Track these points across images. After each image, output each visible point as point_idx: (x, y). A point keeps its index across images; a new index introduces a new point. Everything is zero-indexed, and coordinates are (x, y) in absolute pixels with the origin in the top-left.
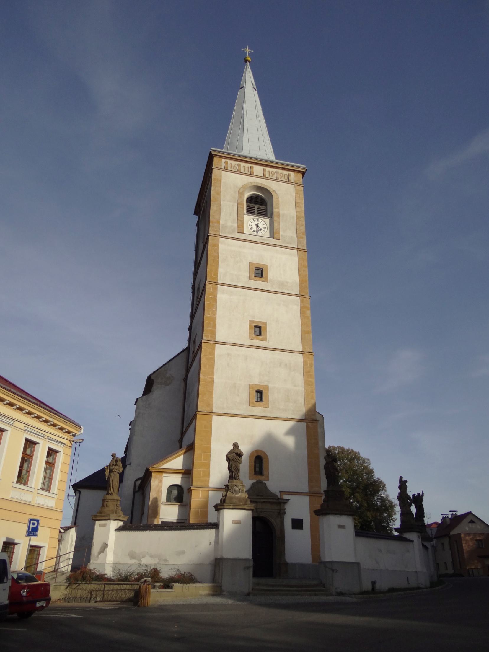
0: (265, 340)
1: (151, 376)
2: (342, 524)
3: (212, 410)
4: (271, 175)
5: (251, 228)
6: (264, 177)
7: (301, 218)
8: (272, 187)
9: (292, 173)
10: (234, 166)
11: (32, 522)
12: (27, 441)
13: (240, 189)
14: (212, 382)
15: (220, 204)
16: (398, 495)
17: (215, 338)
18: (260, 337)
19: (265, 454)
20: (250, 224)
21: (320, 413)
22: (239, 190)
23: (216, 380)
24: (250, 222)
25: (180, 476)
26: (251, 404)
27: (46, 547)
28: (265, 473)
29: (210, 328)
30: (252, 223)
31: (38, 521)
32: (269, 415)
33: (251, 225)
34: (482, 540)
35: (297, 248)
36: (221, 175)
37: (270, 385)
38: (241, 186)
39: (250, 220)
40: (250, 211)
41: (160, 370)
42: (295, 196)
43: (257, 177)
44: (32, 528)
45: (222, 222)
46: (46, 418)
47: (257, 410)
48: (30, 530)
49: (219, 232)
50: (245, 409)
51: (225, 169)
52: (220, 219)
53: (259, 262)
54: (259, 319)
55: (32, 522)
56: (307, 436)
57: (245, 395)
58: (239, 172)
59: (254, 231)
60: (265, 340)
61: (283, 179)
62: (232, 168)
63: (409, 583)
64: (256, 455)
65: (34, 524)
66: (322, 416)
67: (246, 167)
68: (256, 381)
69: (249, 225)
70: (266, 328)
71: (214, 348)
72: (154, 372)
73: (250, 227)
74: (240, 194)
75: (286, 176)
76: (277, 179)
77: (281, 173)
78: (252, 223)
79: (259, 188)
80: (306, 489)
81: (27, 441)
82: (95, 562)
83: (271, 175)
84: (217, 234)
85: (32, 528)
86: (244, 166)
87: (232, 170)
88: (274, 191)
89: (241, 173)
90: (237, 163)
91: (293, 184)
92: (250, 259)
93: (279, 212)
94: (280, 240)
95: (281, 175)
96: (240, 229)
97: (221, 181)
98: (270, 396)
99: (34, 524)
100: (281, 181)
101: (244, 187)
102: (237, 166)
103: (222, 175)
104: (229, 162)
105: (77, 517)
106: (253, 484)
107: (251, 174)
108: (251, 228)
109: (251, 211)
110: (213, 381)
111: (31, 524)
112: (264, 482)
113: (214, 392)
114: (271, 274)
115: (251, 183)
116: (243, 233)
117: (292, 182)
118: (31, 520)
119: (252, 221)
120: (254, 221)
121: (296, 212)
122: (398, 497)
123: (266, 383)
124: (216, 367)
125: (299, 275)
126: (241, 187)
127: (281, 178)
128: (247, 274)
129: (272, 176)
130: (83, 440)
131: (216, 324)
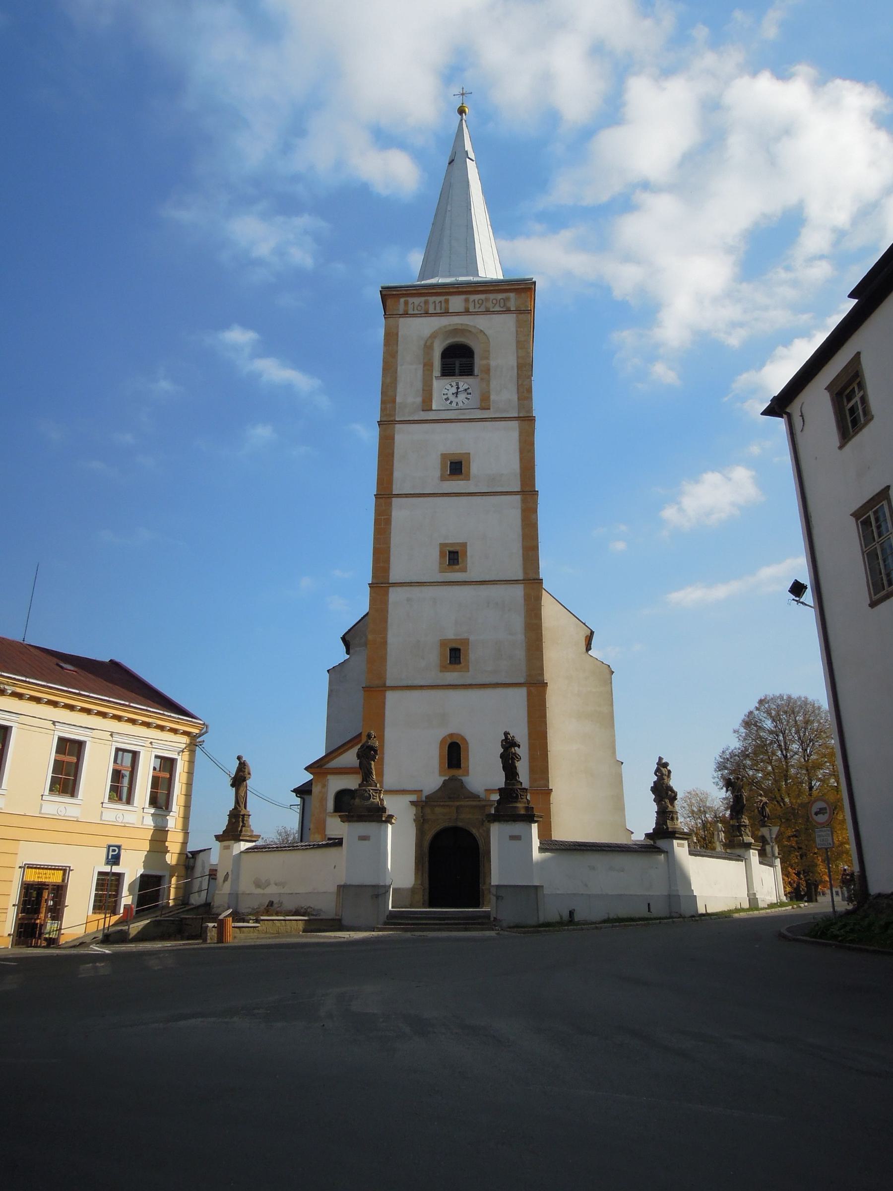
0: (464, 570)
1: (346, 637)
2: (517, 833)
3: (385, 684)
4: (477, 306)
5: (447, 399)
6: (467, 312)
7: (525, 367)
8: (478, 326)
9: (512, 295)
10: (419, 305)
11: (111, 848)
13: (427, 340)
14: (384, 643)
15: (396, 371)
16: (653, 785)
17: (388, 579)
18: (457, 567)
19: (458, 735)
20: (445, 391)
21: (604, 663)
22: (426, 343)
24: (446, 389)
26: (443, 668)
27: (166, 877)
28: (462, 765)
30: (448, 390)
31: (119, 847)
32: (469, 682)
33: (447, 394)
34: (217, 864)
35: (519, 417)
36: (398, 325)
39: (443, 387)
40: (447, 371)
41: (358, 625)
42: (517, 331)
44: (112, 855)
45: (398, 400)
46: (143, 720)
47: (452, 677)
49: (395, 415)
50: (435, 676)
51: (406, 314)
52: (396, 396)
53: (455, 449)
54: (454, 538)
55: (111, 848)
56: (529, 706)
57: (433, 656)
58: (427, 314)
59: (451, 403)
60: (464, 570)
61: (497, 308)
62: (415, 309)
63: (649, 911)
64: (449, 741)
66: (609, 666)
67: (437, 302)
69: (444, 394)
71: (387, 593)
72: (350, 630)
73: (445, 397)
74: (428, 348)
75: (502, 301)
76: (488, 312)
77: (494, 299)
78: (448, 390)
79: (456, 331)
82: (220, 892)
83: (477, 306)
84: (392, 419)
85: (112, 855)
86: (474, 300)
87: (416, 313)
88: (481, 331)
89: (430, 315)
90: (423, 299)
91: (514, 313)
92: (443, 449)
94: (489, 409)
96: (427, 405)
97: (397, 334)
98: (473, 655)
100: (494, 312)
101: (433, 336)
102: (422, 304)
103: (400, 325)
104: (411, 300)
105: (304, 833)
106: (445, 782)
107: (446, 313)
108: (447, 399)
110: (386, 642)
111: (111, 851)
112: (459, 778)
113: (388, 658)
114: (475, 468)
115: (445, 327)
117: (512, 309)
118: (109, 846)
119: (448, 387)
120: (452, 386)
121: (518, 357)
122: (652, 787)
123: (465, 636)
124: (390, 621)
125: (521, 459)
126: (430, 337)
127: (493, 308)
128: (438, 473)
129: (479, 307)
130: (204, 741)
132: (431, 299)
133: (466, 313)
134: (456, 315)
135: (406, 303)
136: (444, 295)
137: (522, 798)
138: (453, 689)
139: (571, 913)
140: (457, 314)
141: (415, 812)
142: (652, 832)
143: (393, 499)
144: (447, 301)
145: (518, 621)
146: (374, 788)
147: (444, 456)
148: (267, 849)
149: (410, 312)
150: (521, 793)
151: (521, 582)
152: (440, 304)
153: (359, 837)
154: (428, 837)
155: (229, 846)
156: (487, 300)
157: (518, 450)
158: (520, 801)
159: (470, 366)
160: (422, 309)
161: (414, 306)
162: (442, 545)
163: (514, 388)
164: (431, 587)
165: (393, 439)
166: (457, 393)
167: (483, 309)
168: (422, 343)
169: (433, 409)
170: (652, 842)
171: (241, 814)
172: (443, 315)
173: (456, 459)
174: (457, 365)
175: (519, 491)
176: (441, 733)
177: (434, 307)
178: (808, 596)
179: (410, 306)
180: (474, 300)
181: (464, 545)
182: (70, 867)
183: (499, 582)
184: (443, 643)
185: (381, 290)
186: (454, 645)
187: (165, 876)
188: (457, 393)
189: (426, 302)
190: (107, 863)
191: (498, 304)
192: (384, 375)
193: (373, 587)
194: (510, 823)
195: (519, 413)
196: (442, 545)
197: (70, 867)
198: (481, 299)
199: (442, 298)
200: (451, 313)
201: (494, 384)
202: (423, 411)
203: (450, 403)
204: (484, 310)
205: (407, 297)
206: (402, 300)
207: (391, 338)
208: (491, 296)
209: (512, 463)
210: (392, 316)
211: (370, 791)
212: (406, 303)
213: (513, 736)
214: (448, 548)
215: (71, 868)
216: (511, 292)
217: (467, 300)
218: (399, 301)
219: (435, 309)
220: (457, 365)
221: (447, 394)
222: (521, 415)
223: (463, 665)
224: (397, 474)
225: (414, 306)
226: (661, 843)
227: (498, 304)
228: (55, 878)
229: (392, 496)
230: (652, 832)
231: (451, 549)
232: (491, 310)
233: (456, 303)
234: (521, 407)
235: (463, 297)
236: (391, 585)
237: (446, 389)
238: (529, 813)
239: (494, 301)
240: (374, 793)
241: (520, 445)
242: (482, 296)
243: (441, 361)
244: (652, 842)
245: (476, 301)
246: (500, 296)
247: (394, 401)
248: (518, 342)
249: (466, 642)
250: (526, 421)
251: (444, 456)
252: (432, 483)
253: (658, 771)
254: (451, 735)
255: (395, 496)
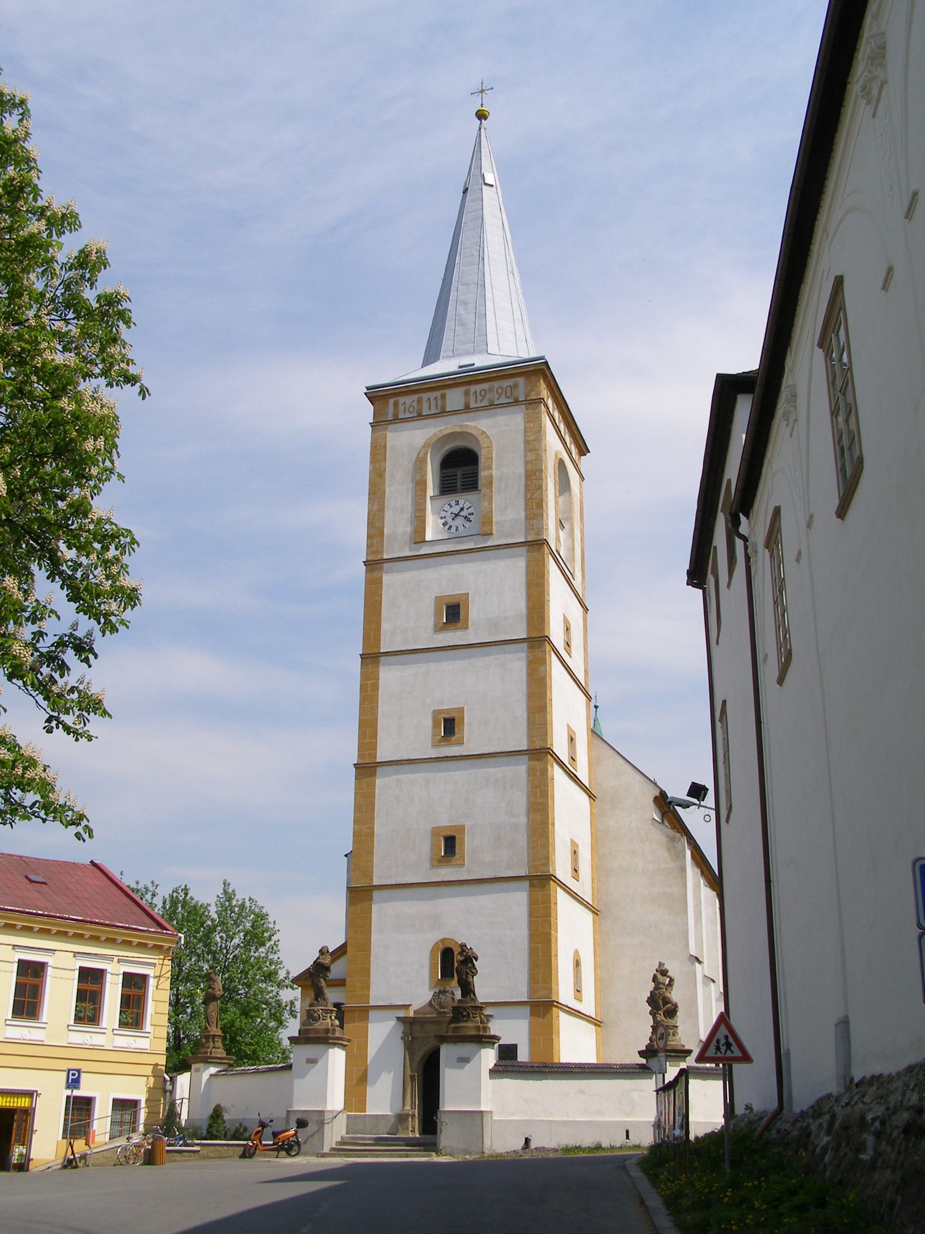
0: (460, 742)
4: (479, 398)
6: (467, 408)
7: (535, 475)
9: (521, 381)
10: (411, 406)
11: (71, 1072)
12: (24, 966)
22: (419, 453)
23: (377, 830)
24: (444, 510)
25: (372, 1003)
29: (368, 740)
31: (79, 1071)
37: (468, 824)
38: (422, 444)
42: (525, 428)
43: (452, 413)
44: (72, 1079)
47: (446, 873)
48: (70, 1081)
52: (384, 527)
53: (451, 590)
57: (424, 847)
58: (420, 416)
60: (460, 742)
61: (503, 400)
62: (407, 411)
63: (627, 1137)
64: (442, 947)
65: (74, 1075)
67: (432, 399)
68: (444, 820)
70: (463, 719)
74: (420, 464)
76: (492, 406)
79: (453, 436)
80: (522, 995)
81: (24, 966)
83: (479, 398)
84: (379, 557)
85: (72, 1079)
86: (476, 392)
90: (415, 397)
92: (437, 591)
93: (491, 476)
95: (500, 391)
98: (469, 845)
99: (74, 1075)
102: (415, 404)
104: (401, 400)
109: (450, 484)
116: (424, 541)
117: (520, 400)
119: (447, 507)
121: (526, 463)
126: (423, 447)
128: (430, 623)
131: (376, 731)
132: (425, 396)
133: (466, 411)
134: (454, 414)
135: (396, 405)
136: (439, 390)
137: (474, 1017)
138: (446, 885)
139: (527, 1141)
140: (455, 412)
141: (402, 1030)
142: (645, 1049)
143: (381, 658)
144: (443, 397)
145: (520, 799)
146: (323, 1008)
147: (438, 599)
148: (234, 1072)
149: (401, 416)
150: (473, 1011)
151: (525, 753)
152: (435, 400)
153: (307, 1059)
154: (418, 1058)
155: (199, 1068)
156: (491, 390)
157: (524, 585)
158: (471, 1020)
159: (475, 480)
160: (414, 410)
161: (405, 408)
162: (436, 713)
163: (521, 503)
164: (423, 764)
165: (381, 583)
166: (457, 515)
167: (485, 403)
168: (414, 456)
169: (427, 539)
170: (644, 1061)
171: (211, 1034)
172: (438, 415)
173: (453, 601)
174: (459, 476)
175: (525, 637)
176: (432, 937)
177: (428, 406)
178: (710, 800)
179: (401, 408)
180: (476, 392)
181: (461, 710)
182: (37, 1091)
183: (500, 755)
184: (435, 832)
185: (366, 391)
186: (449, 833)
187: (140, 1100)
188: (457, 515)
189: (420, 401)
190: (68, 1087)
191: (503, 395)
192: (370, 500)
193: (358, 768)
194: (458, 1044)
195: (526, 537)
196: (436, 713)
197: (37, 1091)
198: (485, 390)
199: (438, 394)
200: (448, 412)
201: (498, 501)
202: (415, 543)
203: (448, 529)
204: (488, 404)
205: (397, 396)
206: (391, 401)
207: (378, 452)
208: (496, 384)
209: (517, 603)
210: (379, 424)
211: (319, 1011)
212: (396, 405)
213: (471, 948)
214: (443, 716)
215: (38, 1092)
216: (518, 377)
217: (467, 394)
218: (388, 403)
219: (430, 409)
220: (459, 476)
221: (445, 517)
222: (529, 539)
223: (457, 856)
224: (385, 626)
225: (405, 408)
226: (653, 1063)
227: (503, 395)
228: (24, 1102)
229: (379, 655)
230: (645, 1049)
231: (446, 716)
232: (496, 403)
233: (455, 399)
234: (528, 528)
235: (462, 389)
236: (378, 764)
237: (444, 510)
238: (481, 1033)
239: (500, 391)
240: (323, 1014)
241: (527, 577)
242: (485, 386)
243: (441, 472)
244: (644, 1061)
245: (478, 393)
246: (506, 383)
247: (382, 534)
248: (527, 442)
249: (461, 829)
250: (536, 546)
251: (438, 599)
252: (427, 637)
253: (655, 979)
254: (443, 940)
255: (383, 654)
